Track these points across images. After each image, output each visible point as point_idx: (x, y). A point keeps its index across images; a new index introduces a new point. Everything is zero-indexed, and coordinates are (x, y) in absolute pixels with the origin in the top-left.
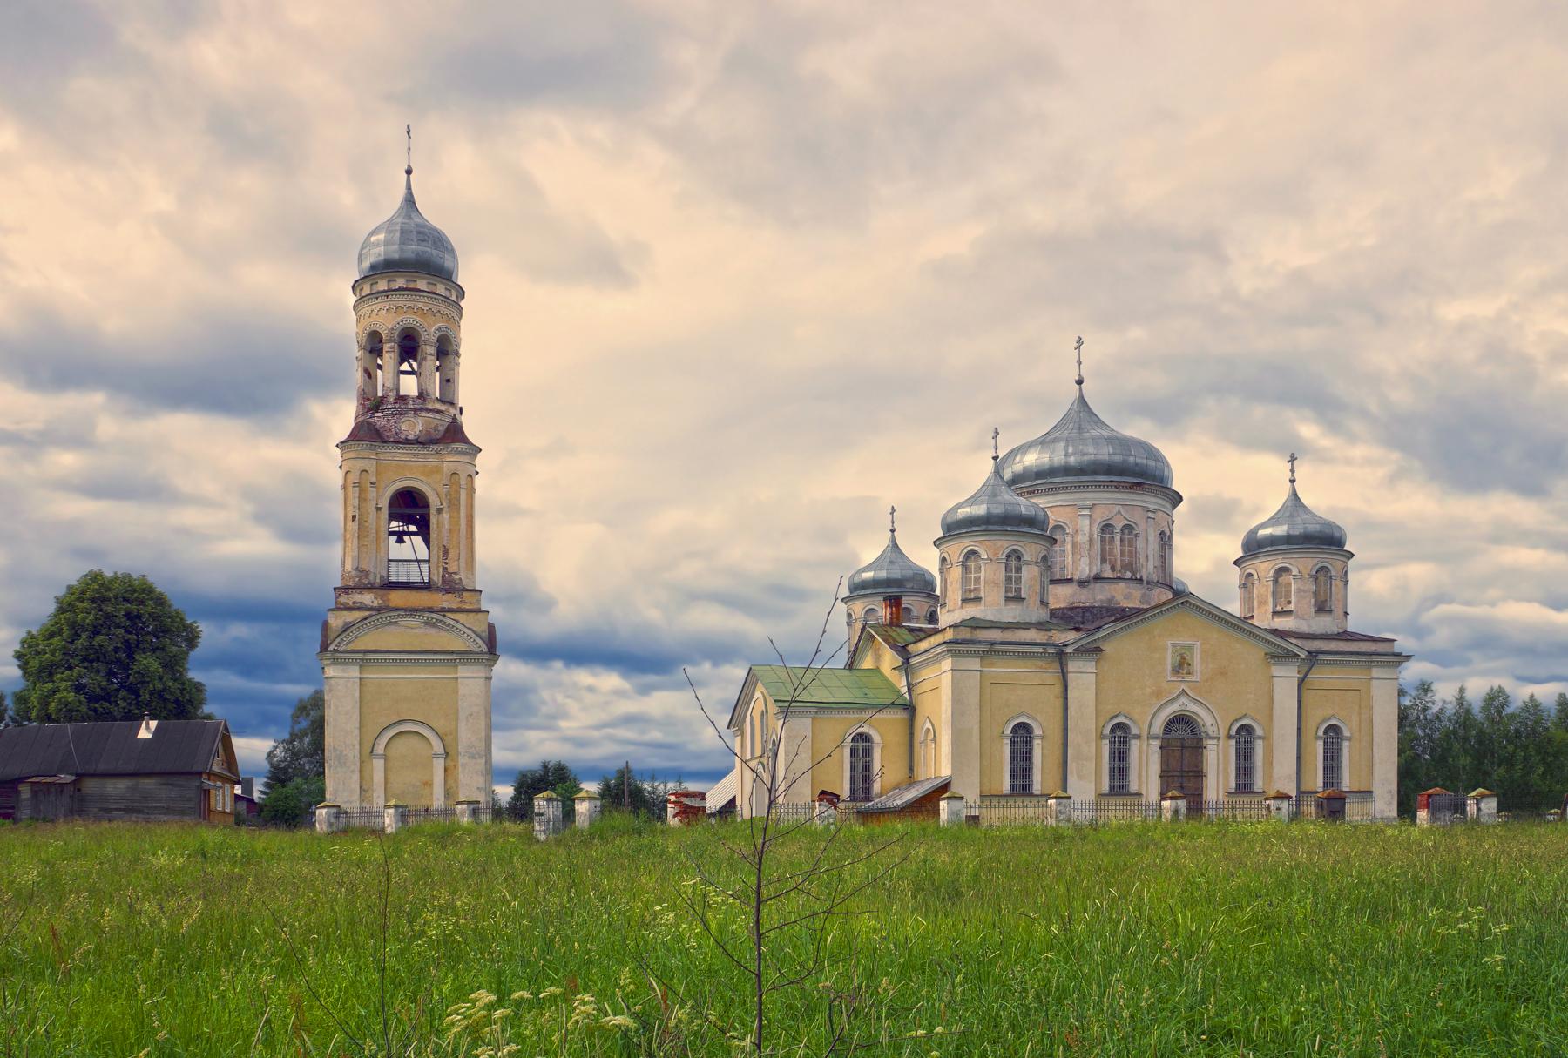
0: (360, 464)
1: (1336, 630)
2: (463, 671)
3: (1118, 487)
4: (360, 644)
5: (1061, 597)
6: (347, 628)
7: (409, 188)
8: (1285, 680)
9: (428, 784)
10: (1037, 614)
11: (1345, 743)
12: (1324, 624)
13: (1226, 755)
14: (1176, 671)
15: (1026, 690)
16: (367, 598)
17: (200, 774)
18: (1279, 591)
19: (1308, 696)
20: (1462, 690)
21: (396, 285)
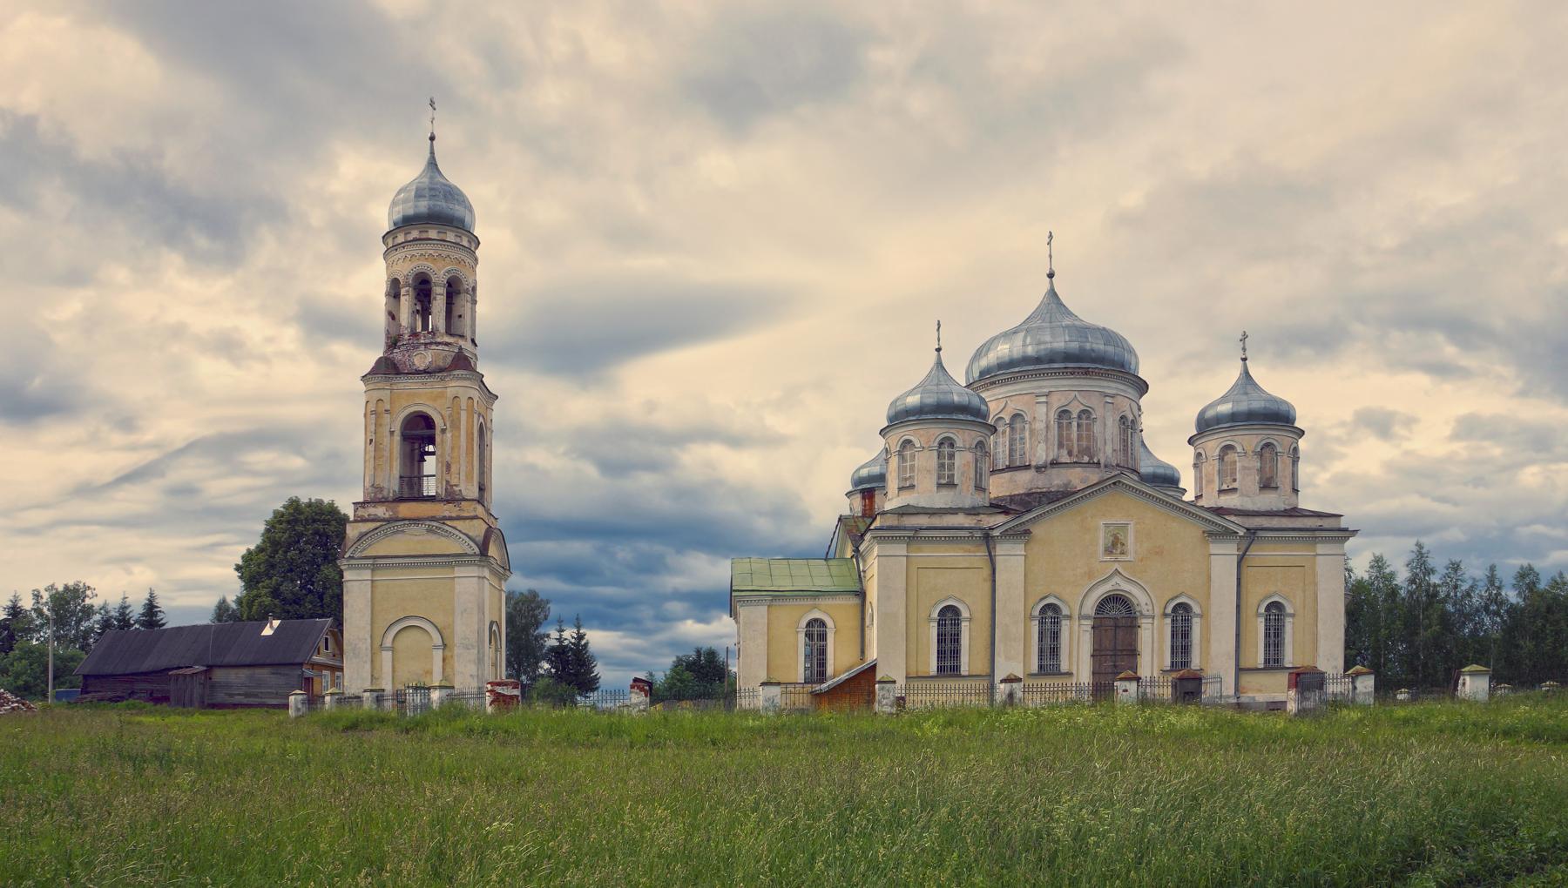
0: (376, 395)
1: (1282, 507)
2: (459, 572)
3: (1073, 373)
4: (369, 552)
5: (999, 487)
6: (362, 536)
7: (432, 153)
8: (1223, 557)
9: (429, 672)
10: (968, 498)
11: (1288, 621)
12: (1269, 501)
13: (1161, 633)
14: (1109, 550)
15: (954, 574)
16: (380, 511)
17: (301, 664)
18: (1227, 471)
19: (1248, 573)
20: (1492, 568)
21: (410, 237)
